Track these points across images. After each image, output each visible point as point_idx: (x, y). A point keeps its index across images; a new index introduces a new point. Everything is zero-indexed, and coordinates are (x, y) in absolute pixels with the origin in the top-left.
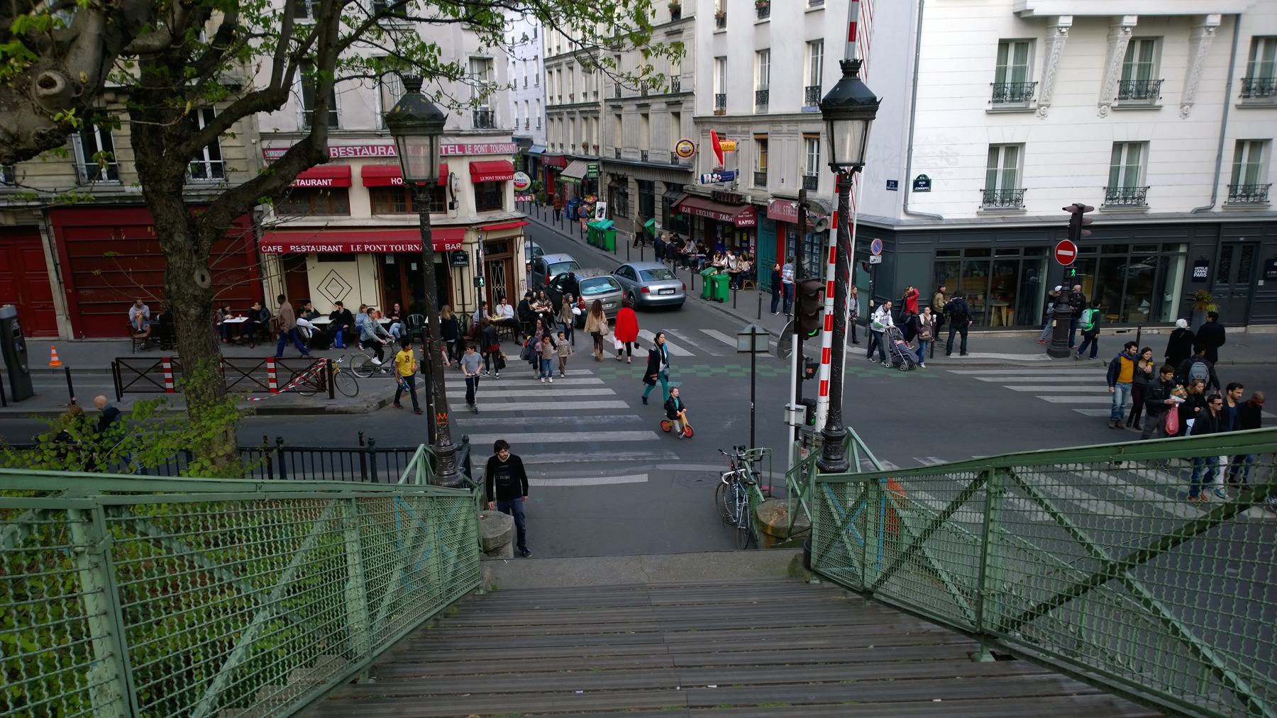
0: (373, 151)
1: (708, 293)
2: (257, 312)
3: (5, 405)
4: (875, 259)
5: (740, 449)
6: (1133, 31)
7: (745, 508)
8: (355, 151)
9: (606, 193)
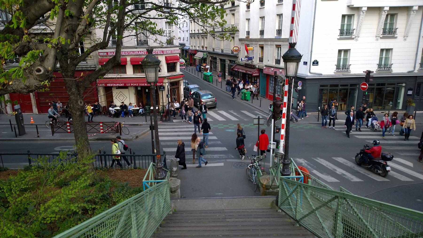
0: (134, 53)
1: (243, 98)
2: (96, 105)
3: (16, 137)
4: (299, 88)
5: (254, 156)
6: (387, 12)
7: (256, 177)
8: (128, 53)
9: (209, 63)
